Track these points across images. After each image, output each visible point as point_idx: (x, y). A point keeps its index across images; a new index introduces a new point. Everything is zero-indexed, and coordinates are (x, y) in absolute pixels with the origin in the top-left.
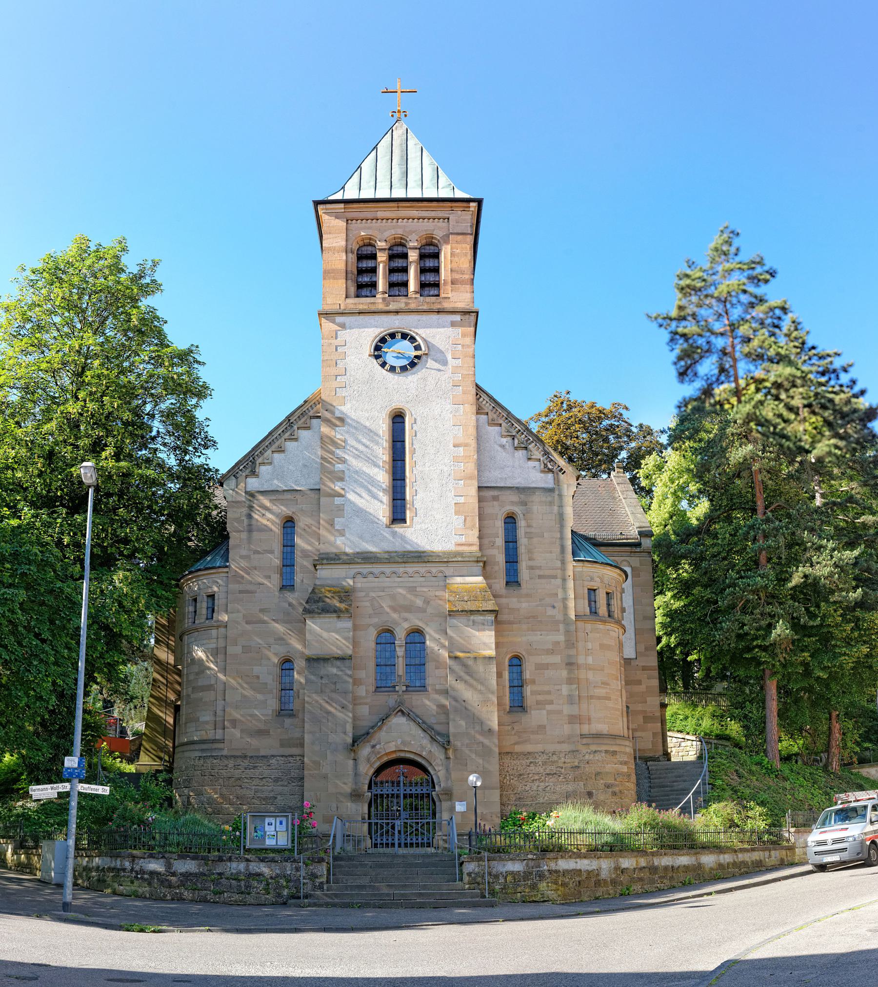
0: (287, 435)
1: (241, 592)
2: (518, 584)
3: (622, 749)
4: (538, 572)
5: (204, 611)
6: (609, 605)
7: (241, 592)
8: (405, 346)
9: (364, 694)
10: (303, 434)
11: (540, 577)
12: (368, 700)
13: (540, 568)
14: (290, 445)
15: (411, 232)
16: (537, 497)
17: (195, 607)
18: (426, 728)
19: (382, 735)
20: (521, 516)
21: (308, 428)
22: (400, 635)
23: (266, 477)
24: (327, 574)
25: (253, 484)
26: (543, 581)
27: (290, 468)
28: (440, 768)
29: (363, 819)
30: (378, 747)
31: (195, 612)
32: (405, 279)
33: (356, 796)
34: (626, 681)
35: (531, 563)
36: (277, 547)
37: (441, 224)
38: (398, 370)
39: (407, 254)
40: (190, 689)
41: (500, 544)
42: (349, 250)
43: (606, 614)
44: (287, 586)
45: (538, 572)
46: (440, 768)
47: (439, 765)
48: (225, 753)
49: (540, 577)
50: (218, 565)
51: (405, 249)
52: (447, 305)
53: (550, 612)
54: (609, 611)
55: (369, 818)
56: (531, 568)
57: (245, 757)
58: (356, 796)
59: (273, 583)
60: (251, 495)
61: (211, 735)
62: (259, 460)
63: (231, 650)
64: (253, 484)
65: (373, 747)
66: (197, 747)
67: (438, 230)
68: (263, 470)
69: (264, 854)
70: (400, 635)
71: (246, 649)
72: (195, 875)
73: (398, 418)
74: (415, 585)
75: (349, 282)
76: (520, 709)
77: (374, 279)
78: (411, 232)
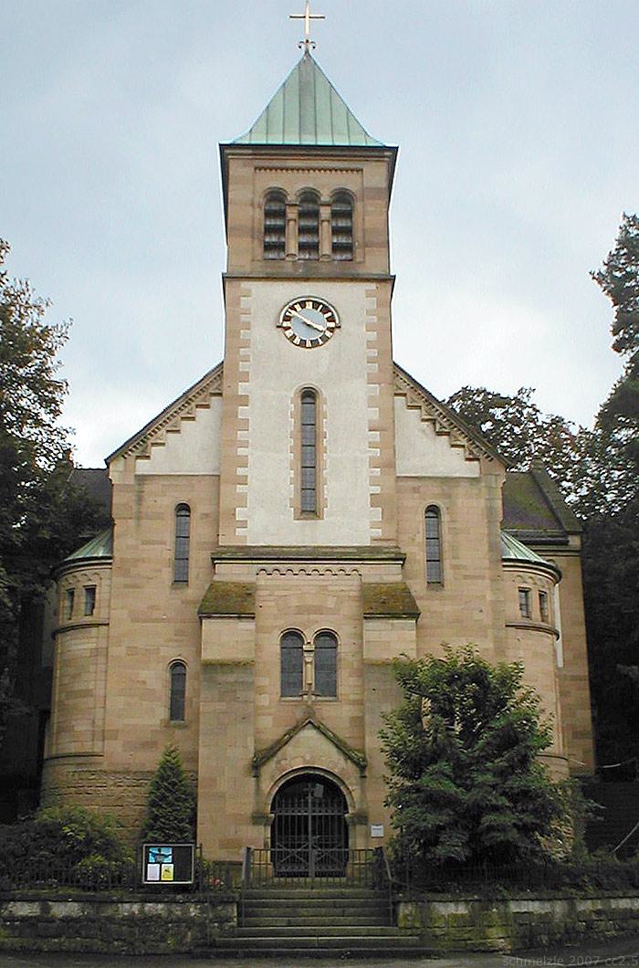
0: (183, 414)
1: (126, 586)
2: (440, 584)
3: (558, 768)
4: (464, 572)
5: (83, 607)
6: (541, 609)
7: (126, 586)
8: (321, 323)
9: (267, 704)
10: (201, 414)
11: (466, 577)
12: (273, 710)
13: (465, 567)
14: (185, 425)
15: (323, 186)
16: (461, 490)
17: (72, 601)
18: (340, 745)
19: (289, 749)
20: (445, 509)
21: (207, 406)
22: (309, 636)
23: (157, 462)
24: (231, 573)
25: (143, 467)
26: (469, 581)
27: (187, 452)
28: (354, 787)
29: (266, 845)
30: (283, 762)
31: (72, 607)
32: (316, 240)
33: (257, 819)
34: (560, 692)
35: (455, 562)
36: (170, 539)
37: (355, 176)
38: (309, 344)
39: (319, 211)
40: (63, 695)
41: (421, 540)
42: (256, 204)
43: (540, 619)
44: (181, 581)
45: (464, 572)
46: (354, 787)
47: (352, 785)
48: (104, 767)
49: (466, 577)
50: (100, 555)
51: (316, 207)
52: (362, 271)
53: (477, 616)
54: (542, 615)
55: (273, 846)
56: (455, 567)
57: (128, 772)
58: (257, 819)
59: (167, 575)
60: (142, 479)
61: (87, 748)
62: (152, 440)
63: (114, 651)
64: (143, 467)
65: (278, 762)
66: (72, 760)
67: (350, 182)
68: (155, 451)
69: (157, 892)
70: (309, 636)
71: (132, 651)
72: (77, 920)
73: (309, 395)
74: (324, 583)
75: (256, 242)
76: (312, 515)
77: (283, 239)
78: (323, 186)
